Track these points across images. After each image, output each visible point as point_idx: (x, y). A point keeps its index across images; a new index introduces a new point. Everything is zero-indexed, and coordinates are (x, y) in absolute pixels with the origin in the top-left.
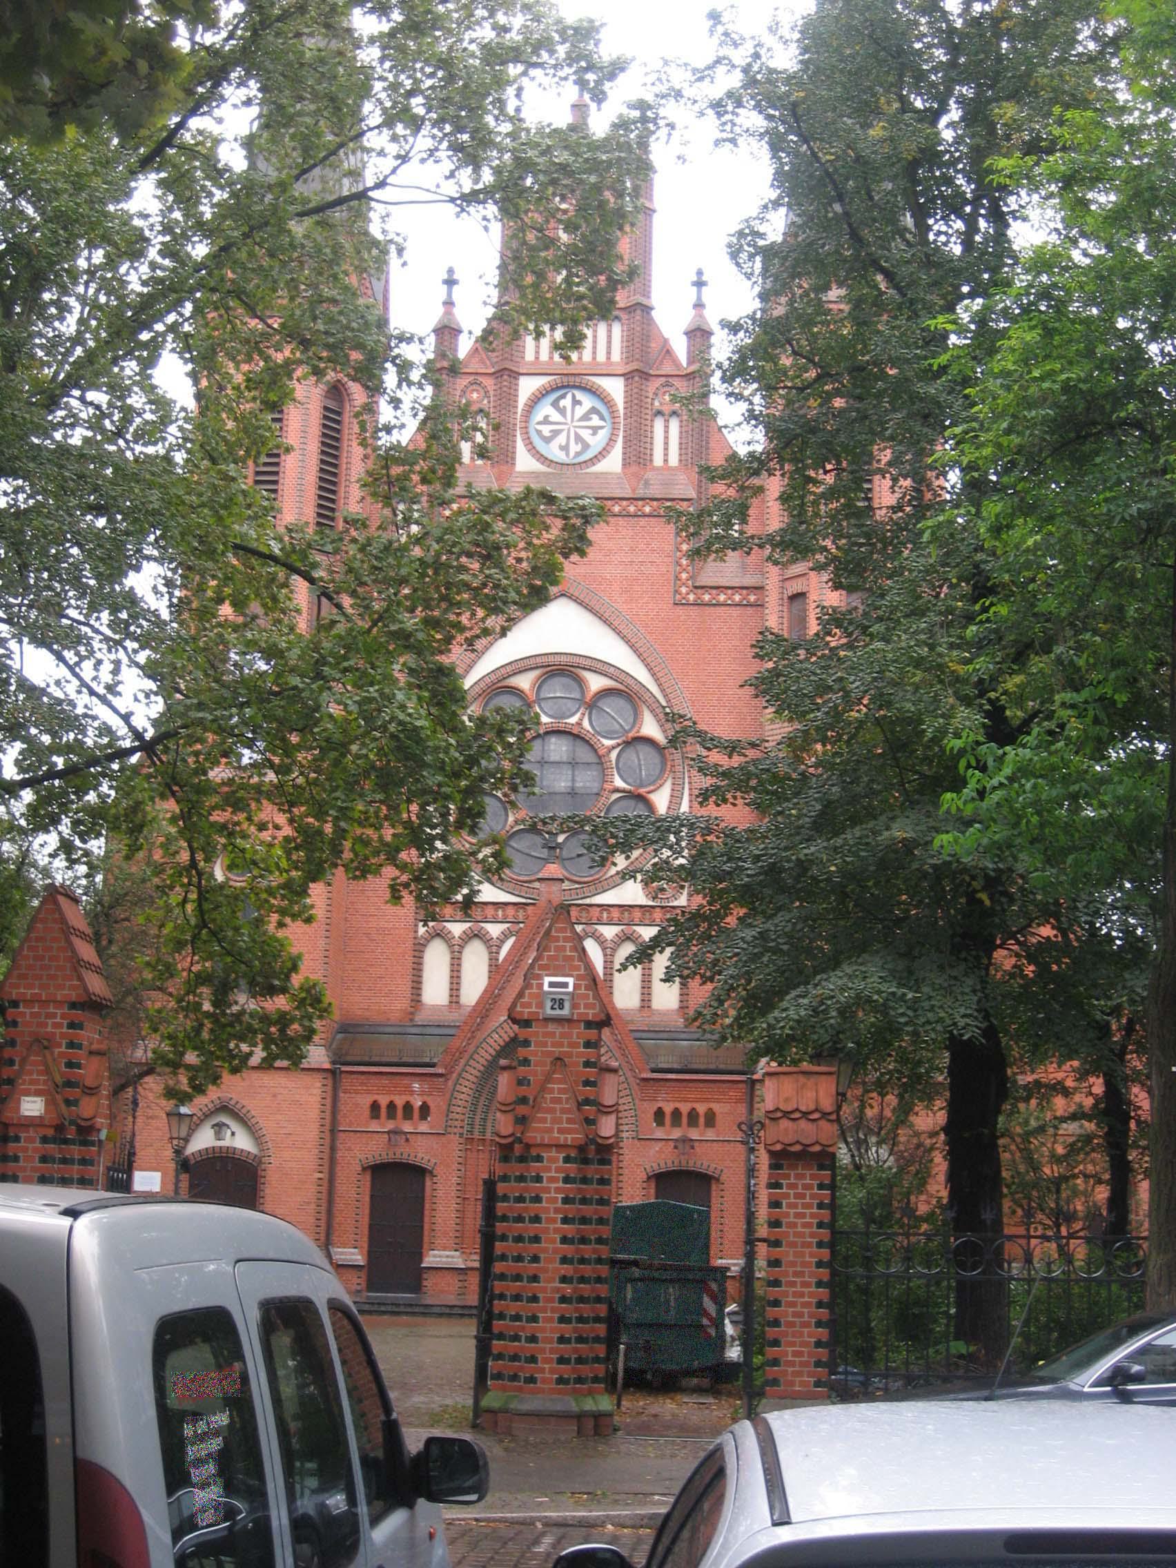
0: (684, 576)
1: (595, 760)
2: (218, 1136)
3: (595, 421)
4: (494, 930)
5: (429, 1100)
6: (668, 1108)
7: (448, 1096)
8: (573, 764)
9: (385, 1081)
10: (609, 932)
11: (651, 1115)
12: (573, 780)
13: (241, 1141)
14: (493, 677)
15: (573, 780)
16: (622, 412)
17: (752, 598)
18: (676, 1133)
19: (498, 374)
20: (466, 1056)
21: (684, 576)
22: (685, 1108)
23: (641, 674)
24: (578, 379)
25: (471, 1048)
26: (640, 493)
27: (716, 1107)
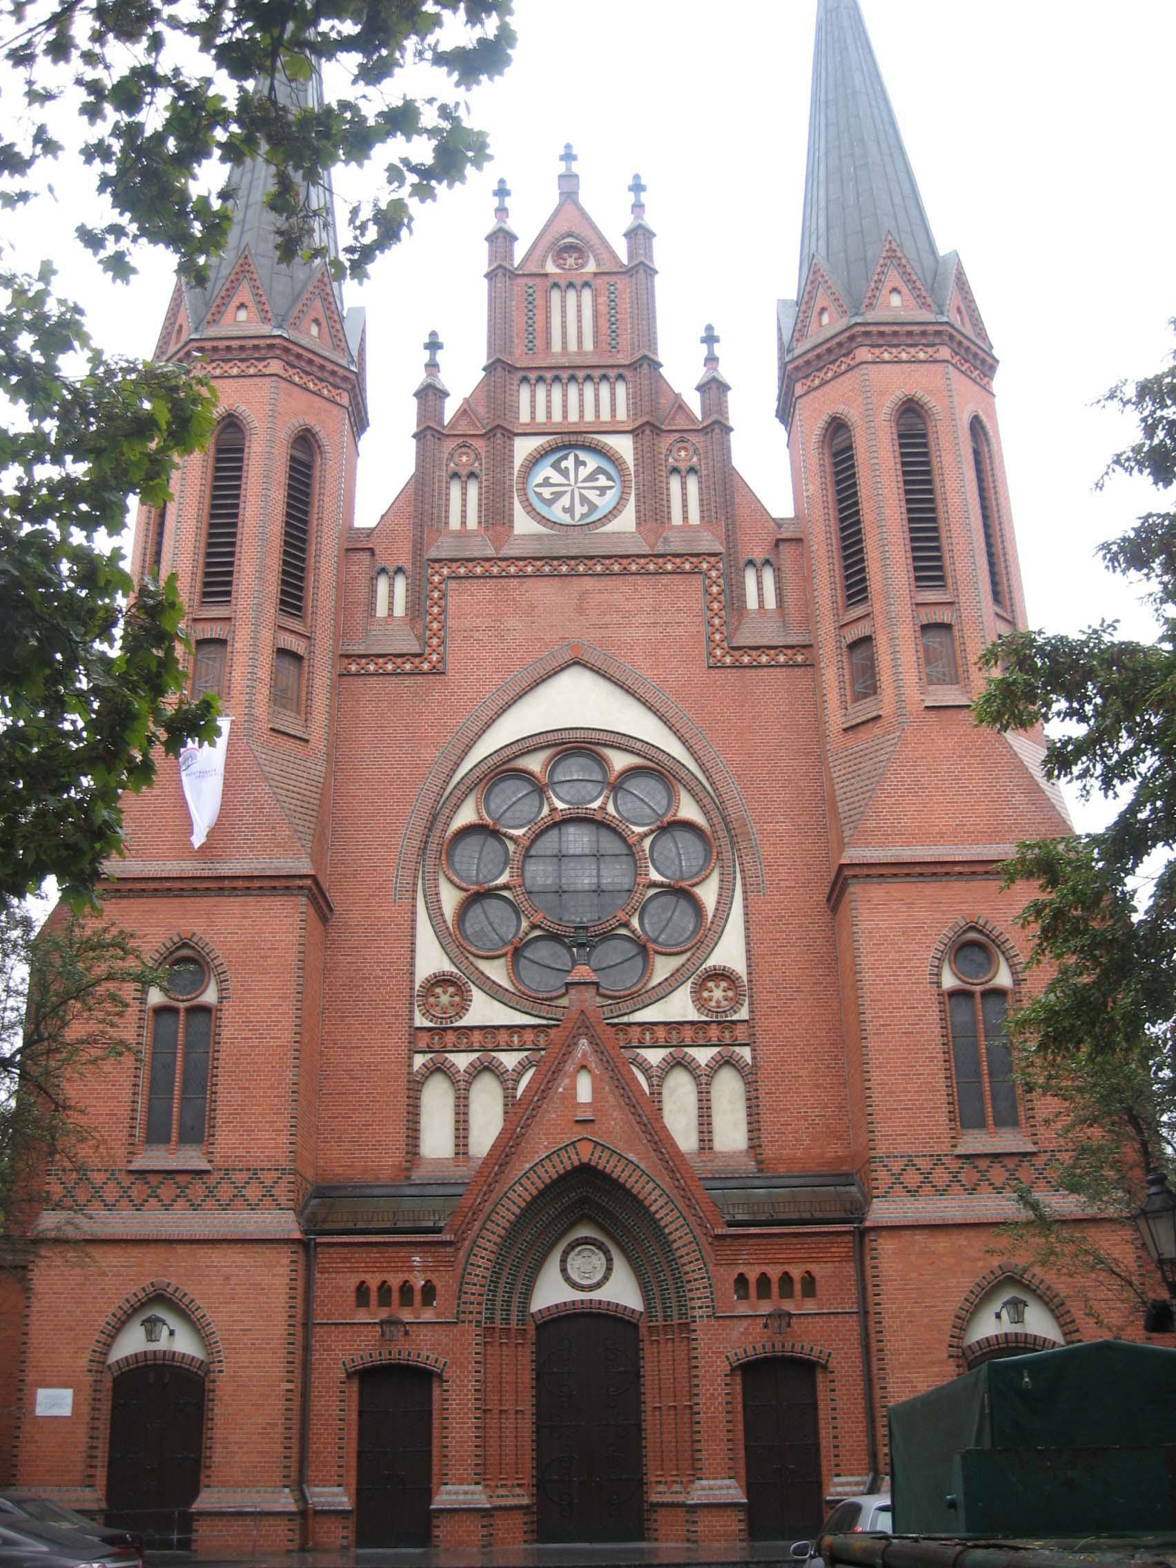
0: (717, 637)
1: (625, 851)
2: (151, 1336)
3: (602, 481)
4: (509, 1060)
5: (434, 1277)
6: (752, 1275)
7: (459, 1272)
8: (598, 856)
9: (375, 1254)
10: (654, 1056)
11: (730, 1285)
12: (599, 876)
13: (184, 1344)
14: (496, 758)
15: (599, 876)
16: (632, 469)
17: (799, 658)
18: (765, 1308)
19: (489, 435)
20: (482, 1217)
21: (717, 637)
22: (774, 1272)
23: (675, 748)
24: (580, 438)
25: (488, 1207)
26: (660, 549)
27: (816, 1269)
